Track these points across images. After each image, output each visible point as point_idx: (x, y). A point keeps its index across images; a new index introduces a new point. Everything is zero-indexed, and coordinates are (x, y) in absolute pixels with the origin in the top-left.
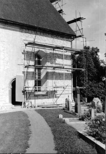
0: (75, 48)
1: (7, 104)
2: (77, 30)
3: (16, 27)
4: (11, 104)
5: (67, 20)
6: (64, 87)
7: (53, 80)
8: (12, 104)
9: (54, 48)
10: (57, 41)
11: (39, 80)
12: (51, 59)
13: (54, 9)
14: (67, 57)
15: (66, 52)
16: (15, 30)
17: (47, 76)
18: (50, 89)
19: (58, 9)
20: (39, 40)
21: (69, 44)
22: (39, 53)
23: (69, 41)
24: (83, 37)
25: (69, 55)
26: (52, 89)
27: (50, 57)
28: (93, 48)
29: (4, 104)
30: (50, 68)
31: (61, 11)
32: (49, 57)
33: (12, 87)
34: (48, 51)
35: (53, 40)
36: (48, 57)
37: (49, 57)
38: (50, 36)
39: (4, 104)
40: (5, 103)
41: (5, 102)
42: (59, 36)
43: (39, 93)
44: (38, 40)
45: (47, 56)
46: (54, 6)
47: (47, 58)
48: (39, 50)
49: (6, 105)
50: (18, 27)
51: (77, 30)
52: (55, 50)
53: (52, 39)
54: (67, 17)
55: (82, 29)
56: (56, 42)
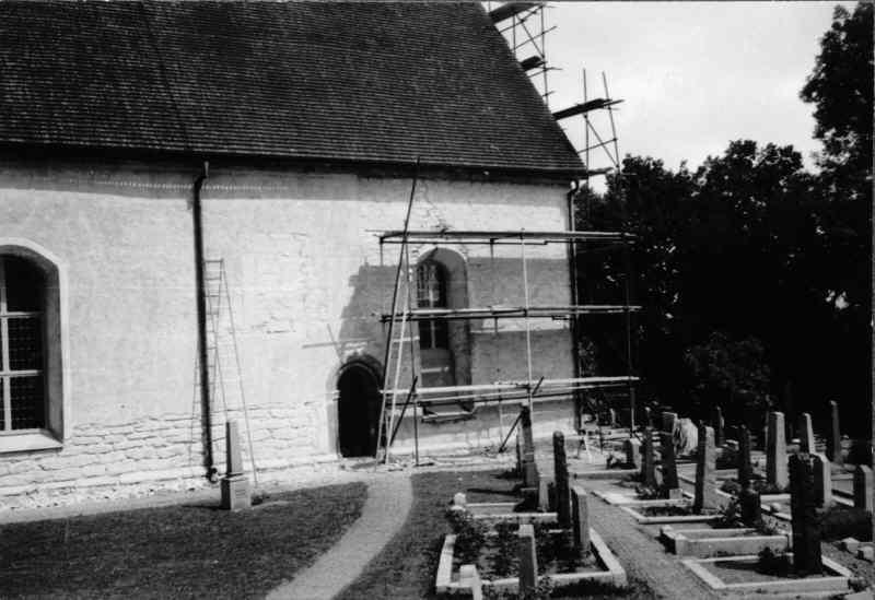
0: (208, 276)
1: (323, 454)
2: (511, 30)
4: (334, 456)
5: (555, 105)
7: (560, 294)
9: (493, 238)
13: (506, 53)
15: (546, 243)
19: (522, 55)
22: (437, 258)
24: (546, 95)
28: (771, 147)
29: (312, 455)
31: (533, 62)
33: (341, 394)
34: (479, 251)
39: (312, 455)
40: (314, 452)
41: (316, 447)
46: (508, 35)
48: (437, 249)
49: (321, 459)
51: (511, 30)
52: (496, 241)
54: (557, 91)
55: (615, 140)
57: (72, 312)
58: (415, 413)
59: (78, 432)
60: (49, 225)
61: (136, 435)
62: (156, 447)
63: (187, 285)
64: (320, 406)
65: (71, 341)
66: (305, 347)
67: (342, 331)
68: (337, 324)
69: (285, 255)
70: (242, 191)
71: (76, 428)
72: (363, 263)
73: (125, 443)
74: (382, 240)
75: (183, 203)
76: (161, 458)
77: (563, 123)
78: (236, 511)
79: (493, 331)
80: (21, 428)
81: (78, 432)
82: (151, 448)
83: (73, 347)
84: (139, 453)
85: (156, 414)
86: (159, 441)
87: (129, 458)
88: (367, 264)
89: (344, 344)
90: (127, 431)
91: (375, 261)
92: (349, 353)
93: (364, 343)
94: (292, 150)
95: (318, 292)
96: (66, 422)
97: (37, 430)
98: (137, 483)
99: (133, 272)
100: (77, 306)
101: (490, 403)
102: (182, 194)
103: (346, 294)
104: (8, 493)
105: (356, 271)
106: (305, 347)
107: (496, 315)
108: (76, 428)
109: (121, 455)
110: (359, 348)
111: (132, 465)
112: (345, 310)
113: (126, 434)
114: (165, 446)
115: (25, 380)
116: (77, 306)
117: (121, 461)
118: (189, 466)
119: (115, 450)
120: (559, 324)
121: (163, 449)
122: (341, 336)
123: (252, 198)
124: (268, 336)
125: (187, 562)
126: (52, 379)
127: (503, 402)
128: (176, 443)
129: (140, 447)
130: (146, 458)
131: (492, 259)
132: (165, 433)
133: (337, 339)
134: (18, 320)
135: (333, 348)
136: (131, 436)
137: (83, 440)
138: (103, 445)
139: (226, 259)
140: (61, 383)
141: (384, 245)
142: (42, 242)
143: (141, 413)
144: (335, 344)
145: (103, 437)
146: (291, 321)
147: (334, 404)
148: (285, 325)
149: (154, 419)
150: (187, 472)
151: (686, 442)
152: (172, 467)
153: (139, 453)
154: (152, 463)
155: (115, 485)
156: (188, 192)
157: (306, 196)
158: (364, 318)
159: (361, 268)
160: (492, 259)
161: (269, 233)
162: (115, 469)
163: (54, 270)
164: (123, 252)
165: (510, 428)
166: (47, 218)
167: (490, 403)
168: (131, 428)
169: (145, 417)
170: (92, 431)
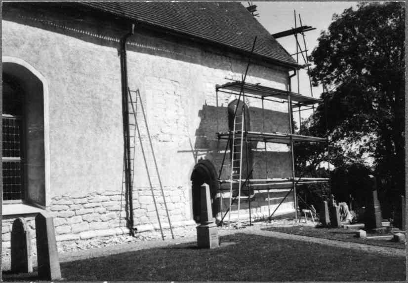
1: (187, 220)
5: (272, 31)
52: (265, 98)
57: (51, 116)
58: (221, 195)
59: (55, 202)
60: (37, 53)
61: (88, 205)
62: (100, 213)
63: (117, 106)
64: (186, 189)
65: (50, 136)
66: (179, 152)
67: (196, 143)
68: (194, 140)
69: (167, 93)
70: (145, 49)
71: (53, 199)
72: (204, 104)
73: (82, 211)
74: (218, 88)
75: (115, 51)
76: (103, 221)
77: (280, 41)
78: (213, 248)
79: (264, 150)
80: (10, 199)
81: (55, 202)
82: (98, 214)
83: (51, 140)
84: (90, 218)
85: (100, 191)
86: (102, 210)
87: (84, 221)
88: (206, 104)
89: (197, 152)
90: (83, 202)
91: (212, 103)
92: (199, 158)
93: (206, 152)
94: (174, 27)
95: (183, 117)
96: (47, 195)
97: (20, 201)
98: (91, 238)
99: (88, 92)
100: (54, 112)
101: (262, 191)
102: (114, 45)
103: (197, 121)
104: (105, 234)
105: (201, 108)
106: (179, 152)
107: (266, 140)
108: (53, 199)
109: (80, 218)
110: (203, 155)
111: (87, 226)
112: (197, 131)
113: (83, 204)
114: (105, 213)
115: (13, 164)
116: (54, 112)
117: (80, 223)
118: (120, 227)
119: (76, 215)
120: (284, 148)
121: (104, 215)
122: (196, 147)
123: (151, 54)
124: (160, 143)
125: (338, 273)
126: (32, 164)
127: (270, 191)
128: (111, 211)
129: (91, 213)
130: (94, 221)
131: (263, 109)
132: (106, 204)
133: (194, 149)
134: (8, 120)
135: (192, 153)
136: (85, 205)
137: (57, 207)
138: (69, 212)
139: (140, 89)
140: (42, 167)
141: (219, 92)
142: (36, 63)
143: (92, 190)
144: (192, 151)
145: (69, 205)
146: (171, 135)
147: (191, 188)
148: (167, 137)
149: (99, 194)
150: (119, 231)
151: (347, 215)
152: (109, 227)
153: (90, 218)
154: (98, 225)
155: (78, 240)
156: (118, 44)
157: (177, 58)
158: (205, 136)
159: (204, 106)
160: (262, 110)
161: (159, 78)
162: (76, 228)
163: (39, 86)
164: (82, 78)
165: (225, 213)
166: (36, 48)
167: (262, 191)
168: (85, 200)
169: (94, 192)
170: (63, 201)
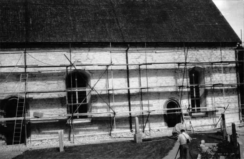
1: (163, 126)
3: (60, 49)
6: (224, 108)
8: (168, 127)
10: (217, 53)
11: (197, 99)
12: (209, 74)
14: (231, 69)
15: (229, 64)
16: (13, 50)
17: (206, 93)
18: (210, 108)
20: (194, 55)
21: (233, 54)
23: (122, 51)
25: (233, 67)
26: (211, 109)
27: (209, 73)
30: (208, 86)
32: (208, 72)
35: (211, 53)
36: (206, 72)
37: (208, 72)
38: (82, 48)
42: (76, 47)
43: (42, 137)
44: (193, 55)
45: (205, 71)
47: (205, 74)
50: (207, 48)
53: (210, 51)
56: (216, 54)
